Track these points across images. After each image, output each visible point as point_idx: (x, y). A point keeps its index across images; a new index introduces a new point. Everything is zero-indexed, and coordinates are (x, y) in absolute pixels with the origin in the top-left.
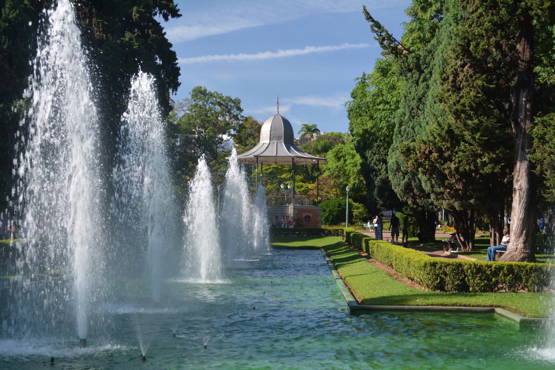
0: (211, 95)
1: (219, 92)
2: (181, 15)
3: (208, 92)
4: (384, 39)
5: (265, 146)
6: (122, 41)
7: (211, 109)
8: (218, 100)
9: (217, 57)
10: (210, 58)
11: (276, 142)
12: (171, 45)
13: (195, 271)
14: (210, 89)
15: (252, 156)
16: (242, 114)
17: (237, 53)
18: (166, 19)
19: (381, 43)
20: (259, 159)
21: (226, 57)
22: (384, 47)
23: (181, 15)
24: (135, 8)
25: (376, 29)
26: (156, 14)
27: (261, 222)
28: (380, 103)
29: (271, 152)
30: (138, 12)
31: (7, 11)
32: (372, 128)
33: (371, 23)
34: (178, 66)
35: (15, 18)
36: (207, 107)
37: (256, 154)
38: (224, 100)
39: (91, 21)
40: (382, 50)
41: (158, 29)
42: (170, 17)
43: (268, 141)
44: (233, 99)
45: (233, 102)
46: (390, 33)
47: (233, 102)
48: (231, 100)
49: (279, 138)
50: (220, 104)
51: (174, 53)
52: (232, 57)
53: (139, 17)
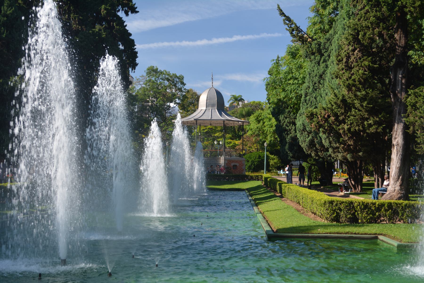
0: (162, 73)
1: (167, 71)
2: (138, 12)
3: (159, 70)
4: (293, 30)
5: (203, 112)
6: (93, 31)
7: (161, 84)
8: (167, 77)
9: (166, 44)
10: (161, 44)
11: (211, 108)
12: (130, 35)
13: (149, 207)
14: (161, 68)
15: (192, 119)
16: (185, 87)
17: (181, 41)
18: (127, 14)
19: (291, 33)
20: (198, 122)
21: (172, 44)
22: (294, 36)
23: (138, 12)
24: (103, 6)
25: (287, 22)
26: (119, 11)
27: (200, 170)
28: (291, 79)
29: (207, 117)
30: (105, 9)
31: (6, 8)
32: (284, 98)
33: (284, 18)
34: (136, 50)
35: (11, 14)
36: (158, 82)
37: (195, 118)
38: (171, 77)
39: (69, 16)
40: (292, 38)
41: (121, 22)
42: (130, 13)
43: (204, 108)
44: (178, 75)
45: (178, 78)
46: (298, 25)
47: (178, 78)
48: (176, 76)
49: (213, 106)
50: (168, 80)
51: (133, 41)
52: (178, 43)
53: (106, 13)
